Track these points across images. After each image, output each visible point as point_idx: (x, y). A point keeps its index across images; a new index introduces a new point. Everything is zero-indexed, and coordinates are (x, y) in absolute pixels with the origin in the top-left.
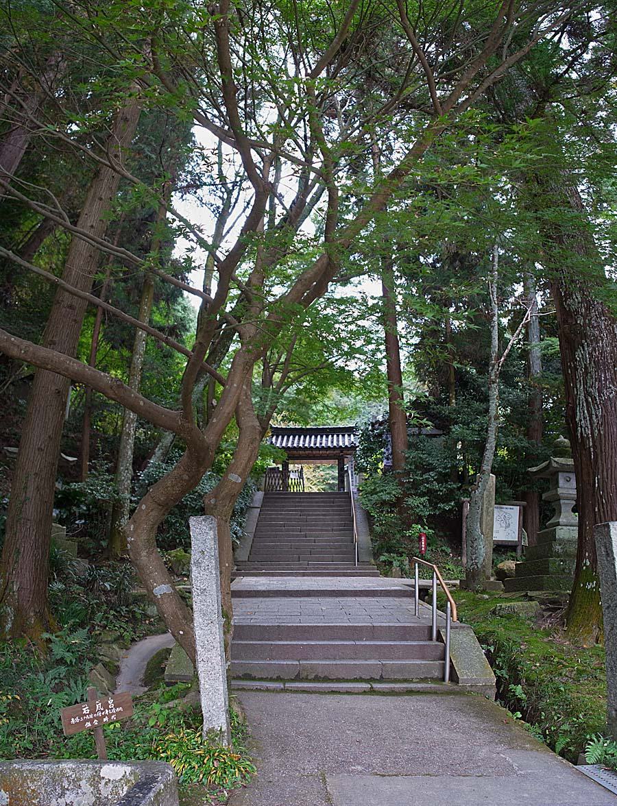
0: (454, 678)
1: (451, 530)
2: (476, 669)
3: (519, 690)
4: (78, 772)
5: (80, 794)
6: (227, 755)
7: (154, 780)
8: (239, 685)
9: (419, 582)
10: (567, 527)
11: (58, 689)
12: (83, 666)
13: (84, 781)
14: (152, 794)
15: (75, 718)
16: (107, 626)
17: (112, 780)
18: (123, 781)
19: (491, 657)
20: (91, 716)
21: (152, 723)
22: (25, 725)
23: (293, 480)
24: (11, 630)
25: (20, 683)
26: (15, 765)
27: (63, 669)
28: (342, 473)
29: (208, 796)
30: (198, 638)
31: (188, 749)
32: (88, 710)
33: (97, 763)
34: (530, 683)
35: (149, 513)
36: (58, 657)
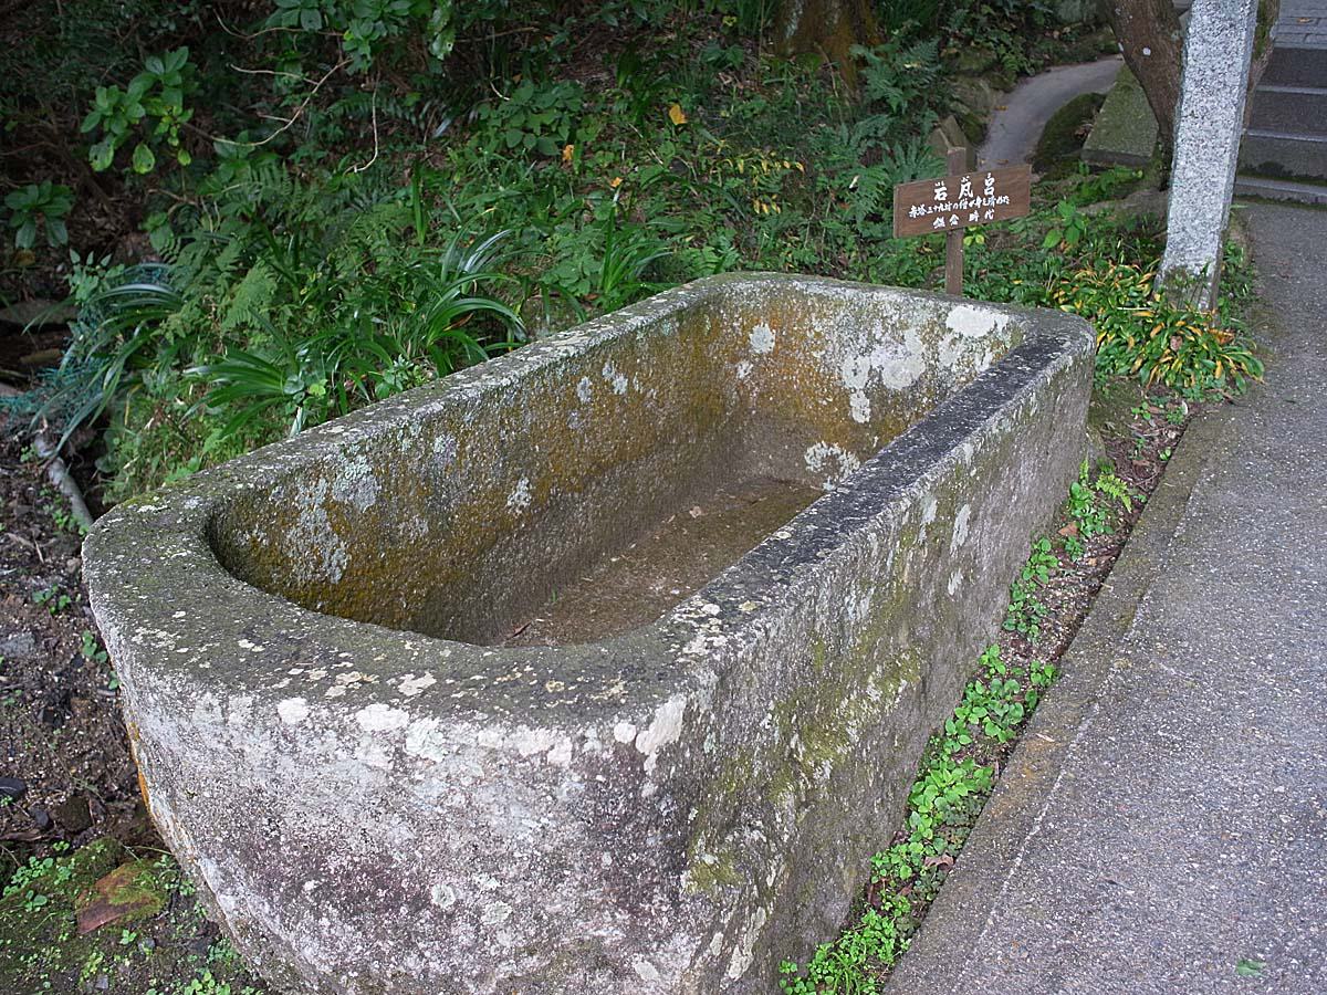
4: (906, 311)
5: (900, 354)
6: (1202, 328)
7: (1056, 346)
8: (1248, 187)
11: (871, 158)
12: (918, 119)
13: (913, 330)
14: (1049, 372)
15: (917, 206)
16: (972, 38)
17: (966, 335)
18: (986, 342)
20: (948, 207)
21: (1050, 242)
22: (806, 222)
23: (277, 177)
24: (797, 37)
25: (806, 141)
26: (795, 283)
27: (884, 120)
29: (1145, 405)
30: (1191, 62)
31: (1120, 305)
32: (945, 195)
33: (944, 299)
36: (877, 96)
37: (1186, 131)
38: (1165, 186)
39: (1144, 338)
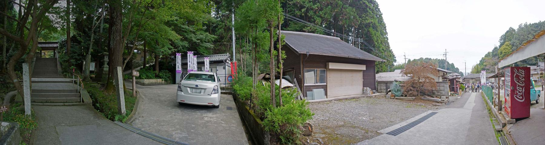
0: (83, 101)
1: (80, 67)
2: (88, 99)
3: (98, 105)
7: (15, 127)
9: (74, 79)
10: (106, 68)
19: (91, 96)
28: (55, 53)
34: (100, 103)
35: (12, 62)
37: (25, 99)
38: (24, 105)
39: (25, 123)
